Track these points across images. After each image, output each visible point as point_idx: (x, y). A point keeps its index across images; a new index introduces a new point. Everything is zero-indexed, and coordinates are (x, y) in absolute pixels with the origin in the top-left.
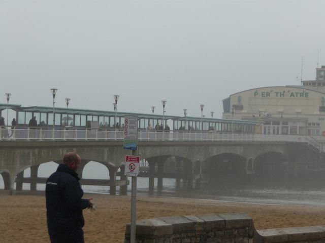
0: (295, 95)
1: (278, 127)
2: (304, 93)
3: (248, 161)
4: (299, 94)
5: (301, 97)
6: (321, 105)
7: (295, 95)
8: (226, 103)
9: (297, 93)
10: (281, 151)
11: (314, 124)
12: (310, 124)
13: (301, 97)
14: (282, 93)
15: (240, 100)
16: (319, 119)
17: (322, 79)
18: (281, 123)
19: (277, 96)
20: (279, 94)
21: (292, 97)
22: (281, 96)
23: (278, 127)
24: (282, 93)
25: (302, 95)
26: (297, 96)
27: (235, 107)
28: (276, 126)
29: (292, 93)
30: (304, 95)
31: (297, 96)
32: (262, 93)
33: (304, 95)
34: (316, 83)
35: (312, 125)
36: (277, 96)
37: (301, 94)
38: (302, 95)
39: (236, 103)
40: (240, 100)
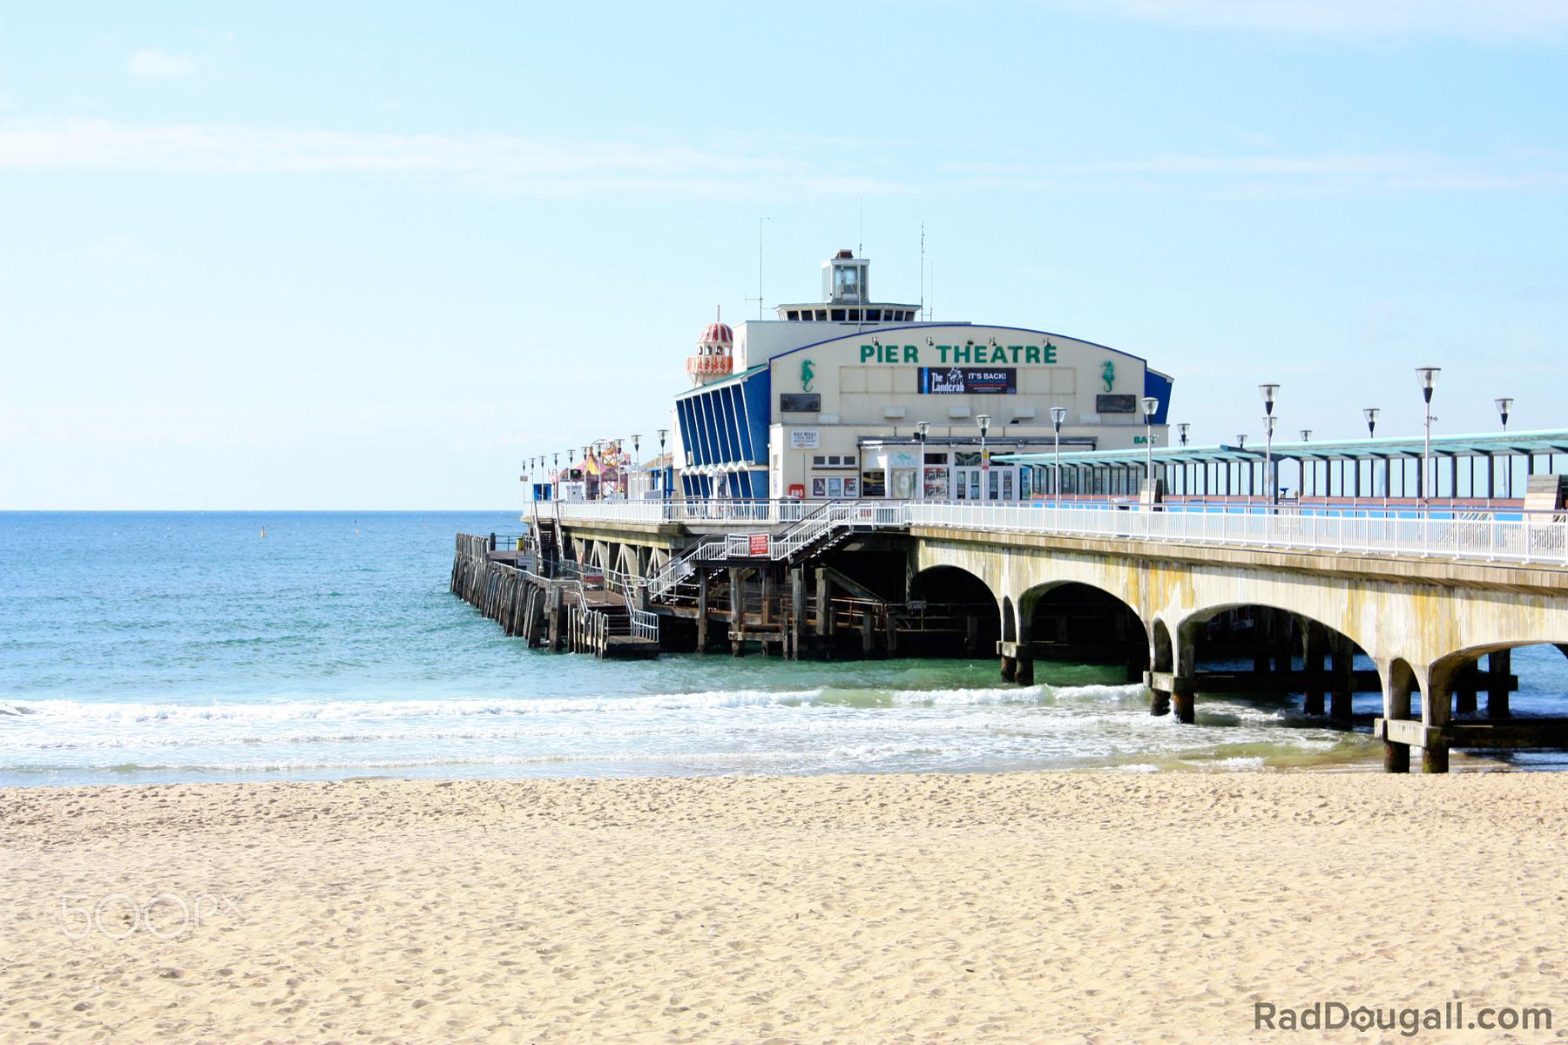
0: (1009, 354)
1: (976, 476)
5: (1028, 361)
7: (1009, 354)
9: (1016, 349)
11: (834, 460)
13: (906, 360)
15: (807, 373)
18: (951, 459)
20: (950, 354)
24: (962, 350)
26: (1015, 360)
28: (969, 470)
29: (1000, 349)
30: (1041, 356)
32: (888, 348)
33: (1041, 356)
35: (842, 464)
36: (944, 360)
39: (795, 387)
40: (807, 373)
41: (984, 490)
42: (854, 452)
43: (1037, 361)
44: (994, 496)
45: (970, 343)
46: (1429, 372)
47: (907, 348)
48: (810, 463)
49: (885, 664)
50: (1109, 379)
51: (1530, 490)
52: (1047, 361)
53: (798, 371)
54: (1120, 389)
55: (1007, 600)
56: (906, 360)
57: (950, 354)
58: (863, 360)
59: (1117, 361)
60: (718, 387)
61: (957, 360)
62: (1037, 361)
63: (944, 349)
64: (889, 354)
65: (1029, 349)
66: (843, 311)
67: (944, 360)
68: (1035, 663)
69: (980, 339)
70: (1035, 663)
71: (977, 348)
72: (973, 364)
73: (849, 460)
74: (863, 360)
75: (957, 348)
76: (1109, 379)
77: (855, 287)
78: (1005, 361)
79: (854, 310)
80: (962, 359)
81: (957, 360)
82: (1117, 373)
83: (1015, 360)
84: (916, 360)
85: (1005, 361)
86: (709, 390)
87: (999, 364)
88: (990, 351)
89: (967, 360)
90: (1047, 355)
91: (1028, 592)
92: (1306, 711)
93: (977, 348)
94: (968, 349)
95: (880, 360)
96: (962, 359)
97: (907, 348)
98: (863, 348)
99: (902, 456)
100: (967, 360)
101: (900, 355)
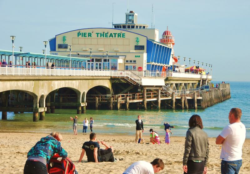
0: (114, 35)
2: (122, 34)
3: (39, 98)
5: (118, 37)
7: (114, 35)
8: (53, 43)
9: (115, 34)
10: (107, 84)
11: (131, 61)
12: (127, 61)
13: (89, 36)
14: (102, 34)
16: (136, 56)
17: (131, 22)
18: (103, 60)
19: (98, 36)
20: (99, 35)
21: (111, 37)
22: (101, 37)
23: (100, 64)
24: (102, 34)
25: (119, 35)
26: (115, 37)
27: (60, 46)
28: (98, 63)
29: (111, 34)
30: (121, 36)
31: (115, 37)
32: (84, 33)
33: (121, 36)
34: (132, 28)
36: (98, 36)
37: (118, 34)
38: (119, 35)
39: (61, 43)
40: (64, 39)
41: (95, 67)
43: (121, 37)
44: (97, 68)
46: (21, 48)
47: (89, 33)
50: (137, 41)
51: (168, 64)
52: (123, 37)
54: (140, 44)
55: (84, 93)
56: (89, 36)
58: (78, 36)
60: (163, 45)
62: (121, 37)
63: (98, 34)
64: (84, 35)
66: (130, 26)
68: (8, 113)
70: (8, 113)
74: (78, 36)
75: (101, 34)
76: (137, 41)
77: (131, 20)
79: (129, 25)
84: (91, 36)
85: (113, 37)
86: (160, 44)
88: (109, 35)
90: (123, 35)
93: (123, 34)
95: (82, 36)
96: (102, 36)
97: (89, 33)
99: (113, 60)
101: (87, 35)
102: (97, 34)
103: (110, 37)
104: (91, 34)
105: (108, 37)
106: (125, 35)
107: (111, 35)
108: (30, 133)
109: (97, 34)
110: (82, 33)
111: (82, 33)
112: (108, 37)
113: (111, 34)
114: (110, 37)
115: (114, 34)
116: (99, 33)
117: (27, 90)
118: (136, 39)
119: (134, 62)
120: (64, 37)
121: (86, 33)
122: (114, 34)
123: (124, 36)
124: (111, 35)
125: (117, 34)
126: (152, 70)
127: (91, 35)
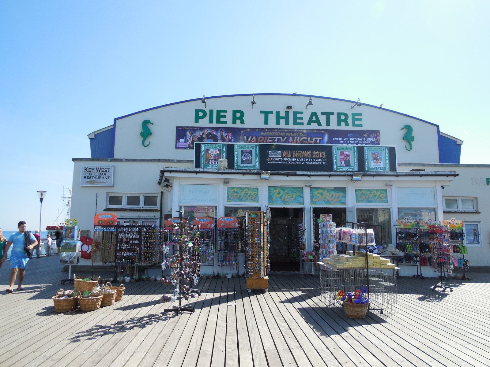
0: (323, 119)
4: (333, 119)
6: (40, 197)
7: (323, 119)
9: (328, 115)
11: (133, 200)
14: (282, 114)
20: (272, 118)
24: (282, 114)
32: (219, 112)
35: (124, 205)
36: (266, 122)
42: (154, 190)
45: (289, 108)
46: (42, 193)
47: (235, 112)
48: (103, 203)
49: (476, 266)
53: (140, 129)
57: (272, 118)
59: (414, 125)
61: (278, 123)
63: (266, 114)
64: (219, 116)
65: (339, 115)
67: (266, 122)
68: (264, 114)
69: (298, 105)
71: (295, 113)
72: (291, 126)
73: (149, 200)
75: (278, 113)
78: (319, 124)
80: (282, 121)
81: (278, 123)
82: (414, 134)
83: (328, 123)
85: (319, 124)
87: (314, 126)
88: (306, 117)
89: (287, 123)
91: (19, 223)
92: (145, 275)
93: (295, 113)
94: (287, 113)
96: (282, 121)
97: (235, 112)
98: (197, 112)
100: (287, 123)
102: (263, 115)
103: (309, 124)
104: (242, 114)
105: (302, 124)
106: (224, 117)
107: (314, 119)
108: (463, 197)
109: (263, 115)
110: (211, 112)
111: (211, 112)
112: (302, 124)
113: (314, 114)
114: (309, 124)
115: (323, 113)
116: (272, 112)
117: (23, 221)
118: (405, 131)
119: (146, 203)
120: (146, 123)
121: (302, 113)
122: (323, 113)
123: (222, 119)
124: (314, 119)
125: (274, 113)
126: (112, 232)
127: (244, 118)
